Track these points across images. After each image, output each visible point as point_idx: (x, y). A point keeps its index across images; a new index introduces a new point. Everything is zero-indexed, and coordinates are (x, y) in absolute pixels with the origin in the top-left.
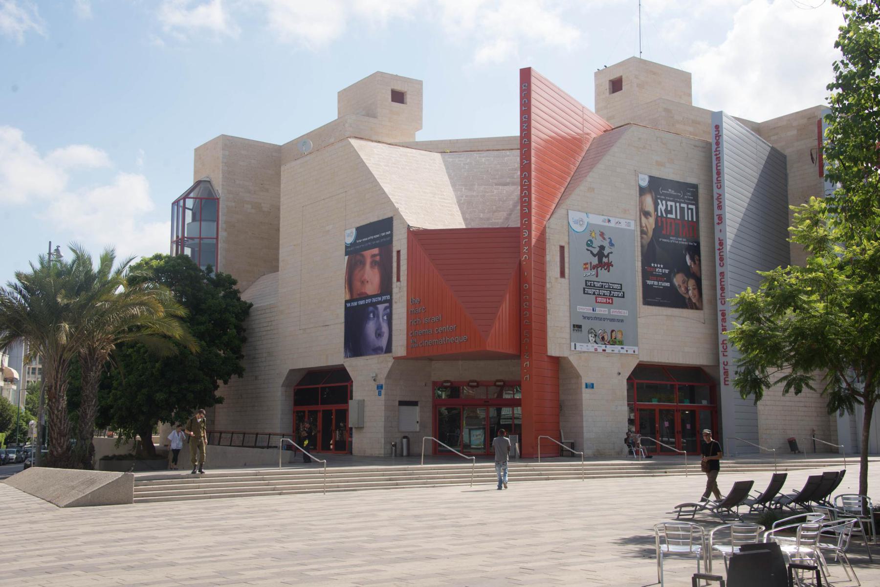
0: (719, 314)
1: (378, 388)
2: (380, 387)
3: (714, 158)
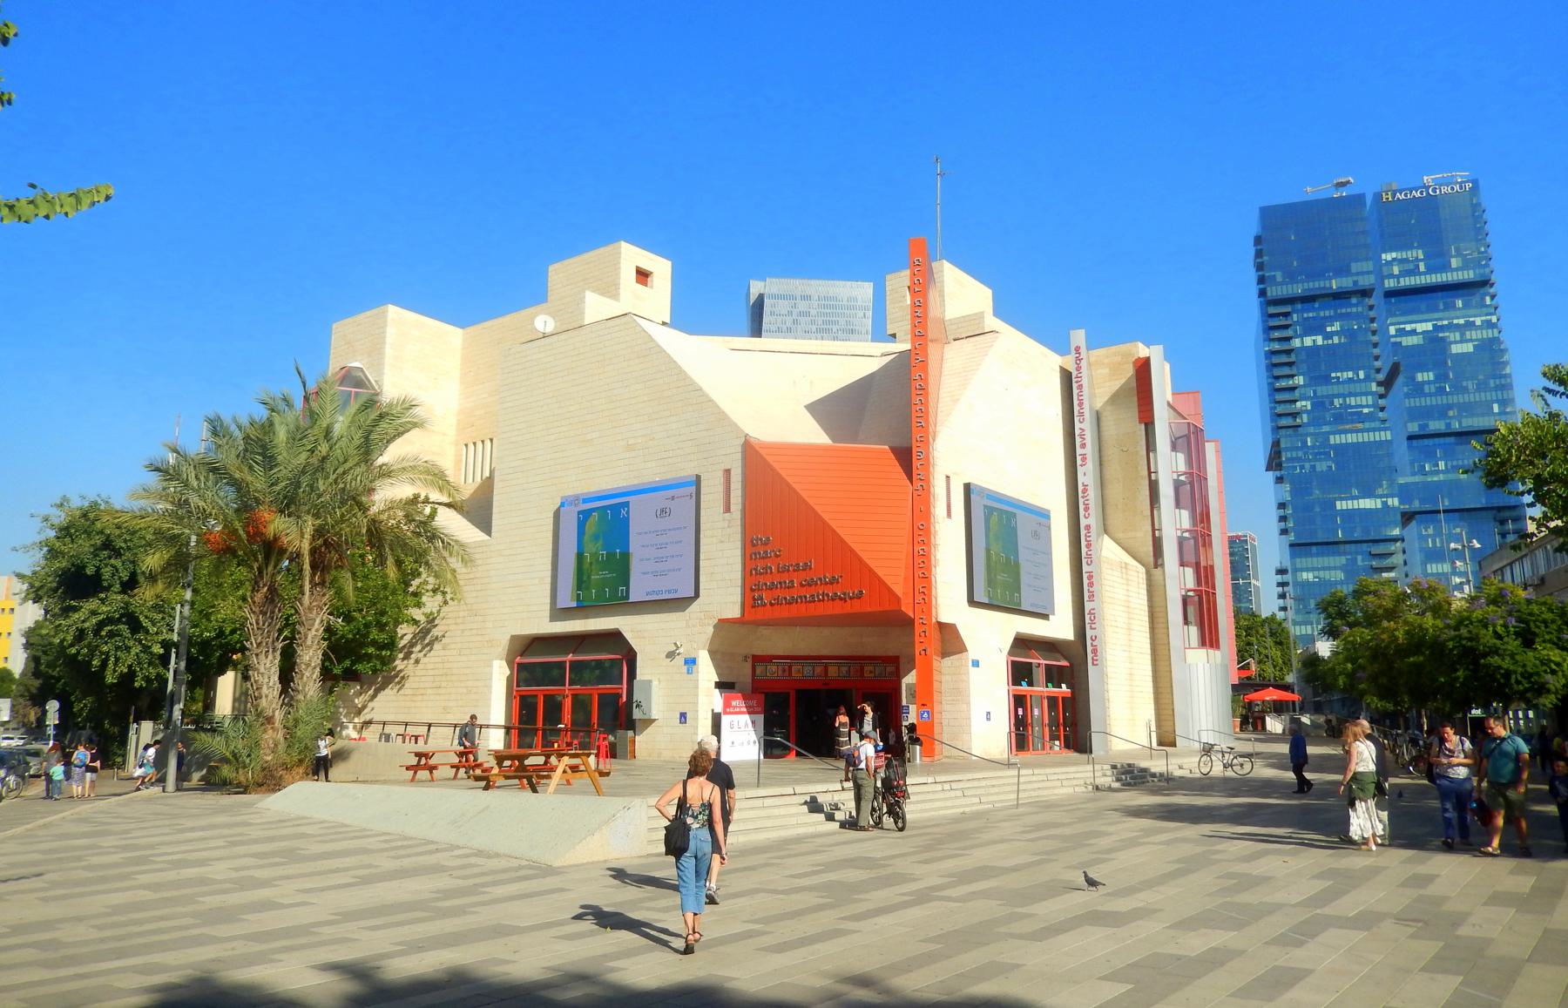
0: (1085, 576)
3: (1075, 386)
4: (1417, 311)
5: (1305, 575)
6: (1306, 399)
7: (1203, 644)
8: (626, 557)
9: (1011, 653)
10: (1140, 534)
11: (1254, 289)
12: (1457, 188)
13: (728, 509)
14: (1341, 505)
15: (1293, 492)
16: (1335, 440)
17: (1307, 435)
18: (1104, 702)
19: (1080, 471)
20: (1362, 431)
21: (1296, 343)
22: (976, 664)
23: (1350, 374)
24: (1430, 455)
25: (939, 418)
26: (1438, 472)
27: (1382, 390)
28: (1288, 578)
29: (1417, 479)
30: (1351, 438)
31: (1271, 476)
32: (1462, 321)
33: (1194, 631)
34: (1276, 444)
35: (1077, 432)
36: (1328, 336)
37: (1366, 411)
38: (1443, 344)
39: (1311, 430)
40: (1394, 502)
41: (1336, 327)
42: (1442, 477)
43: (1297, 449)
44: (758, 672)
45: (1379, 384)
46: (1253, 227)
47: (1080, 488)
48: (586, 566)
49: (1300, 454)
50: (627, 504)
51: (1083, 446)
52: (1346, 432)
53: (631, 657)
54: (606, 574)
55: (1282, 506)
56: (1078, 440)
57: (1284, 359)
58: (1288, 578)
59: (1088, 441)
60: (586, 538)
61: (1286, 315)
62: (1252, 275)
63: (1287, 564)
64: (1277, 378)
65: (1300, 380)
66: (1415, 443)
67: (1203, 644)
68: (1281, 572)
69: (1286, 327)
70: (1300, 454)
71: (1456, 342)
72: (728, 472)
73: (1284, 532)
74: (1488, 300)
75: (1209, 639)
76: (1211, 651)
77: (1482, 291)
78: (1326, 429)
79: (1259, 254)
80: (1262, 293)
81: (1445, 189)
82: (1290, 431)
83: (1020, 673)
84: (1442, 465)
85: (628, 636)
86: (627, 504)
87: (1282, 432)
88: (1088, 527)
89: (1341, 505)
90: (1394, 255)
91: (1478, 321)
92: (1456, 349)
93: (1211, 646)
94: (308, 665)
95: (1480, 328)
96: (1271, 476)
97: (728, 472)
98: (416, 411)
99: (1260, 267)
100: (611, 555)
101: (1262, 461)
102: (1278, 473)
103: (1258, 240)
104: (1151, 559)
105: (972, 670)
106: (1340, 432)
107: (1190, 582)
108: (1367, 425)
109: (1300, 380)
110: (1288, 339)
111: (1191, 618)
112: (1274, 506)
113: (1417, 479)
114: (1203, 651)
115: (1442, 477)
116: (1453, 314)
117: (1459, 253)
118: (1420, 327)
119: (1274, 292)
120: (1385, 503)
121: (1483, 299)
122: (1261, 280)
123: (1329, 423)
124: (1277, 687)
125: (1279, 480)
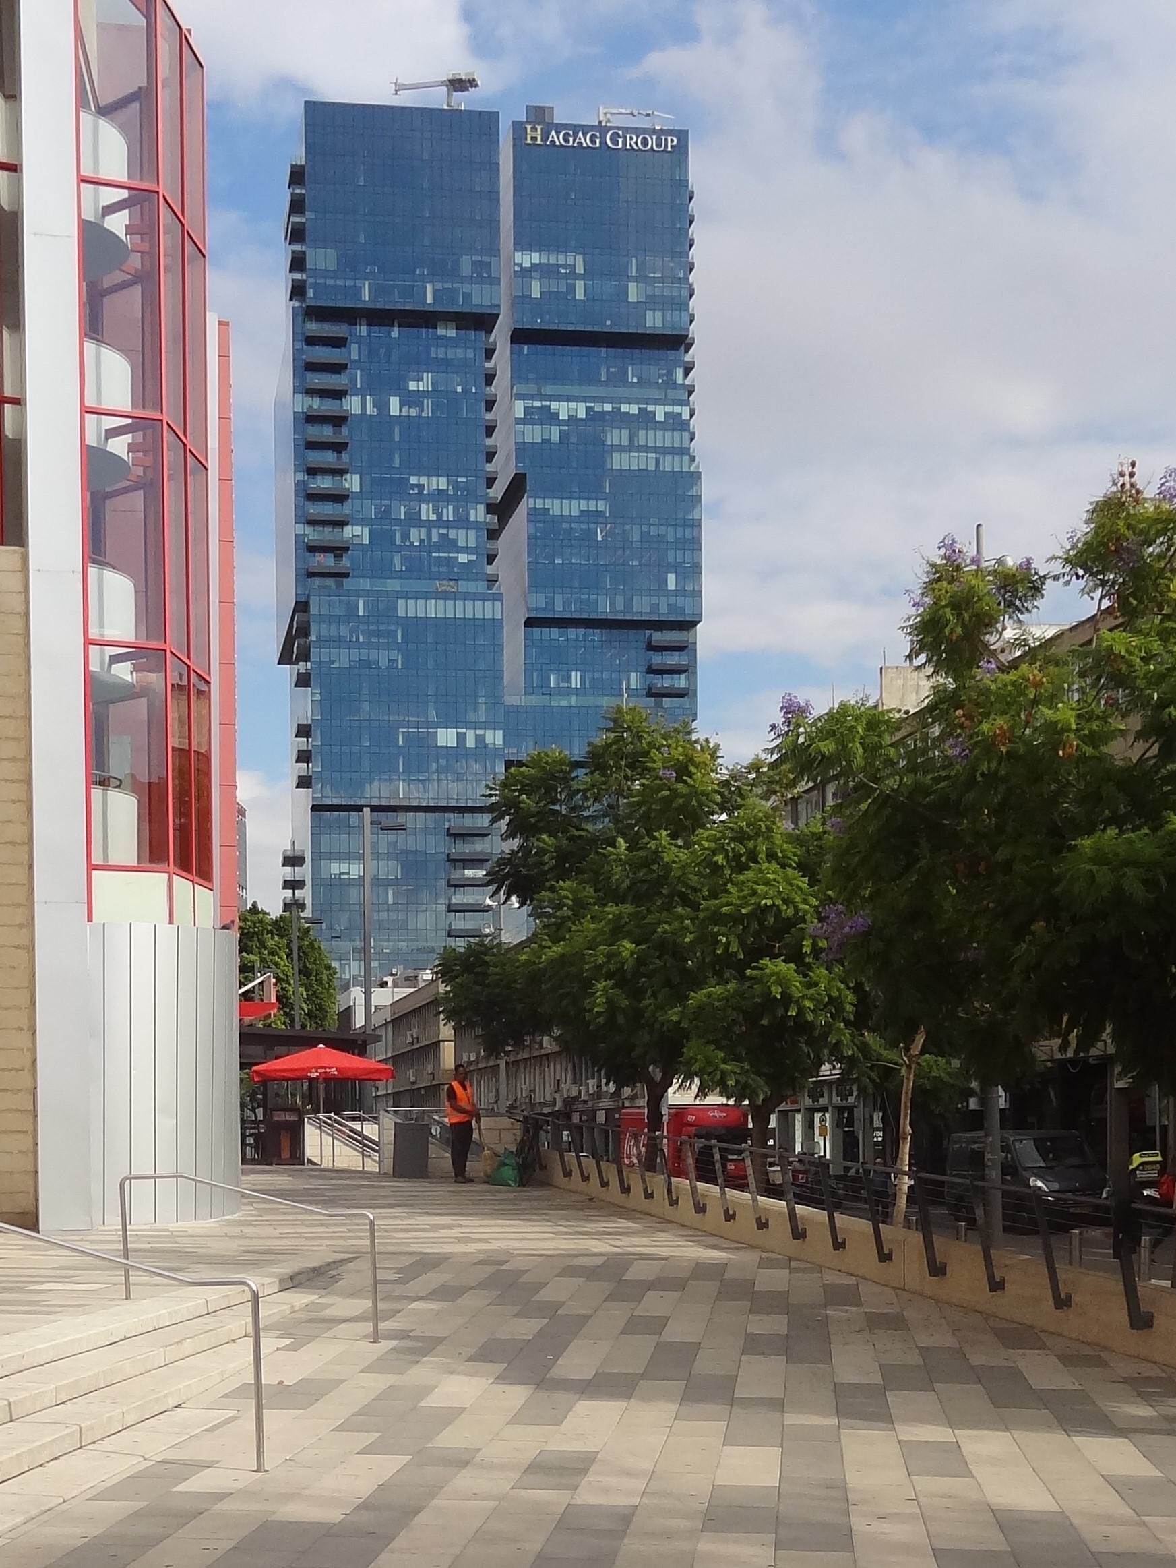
4: (558, 378)
5: (335, 868)
6: (362, 522)
7: (153, 852)
11: (282, 282)
12: (652, 142)
15: (327, 704)
16: (407, 609)
17: (358, 594)
20: (455, 596)
21: (353, 405)
24: (560, 661)
26: (569, 691)
27: (493, 520)
28: (304, 872)
29: (534, 700)
30: (434, 609)
31: (288, 672)
32: (634, 409)
33: (123, 810)
34: (301, 607)
36: (409, 399)
37: (463, 558)
38: (602, 450)
39: (365, 584)
40: (496, 738)
42: (574, 700)
43: (338, 620)
45: (490, 509)
49: (344, 630)
52: (426, 596)
55: (303, 731)
57: (326, 433)
58: (304, 872)
61: (339, 343)
64: (312, 472)
65: (353, 483)
66: (537, 632)
67: (153, 852)
68: (292, 860)
69: (339, 343)
70: (344, 630)
71: (620, 449)
74: (679, 372)
76: (182, 885)
77: (671, 354)
78: (393, 585)
79: (297, 206)
80: (297, 291)
81: (633, 141)
82: (330, 582)
84: (576, 679)
87: (317, 581)
90: (536, 258)
91: (660, 413)
92: (618, 461)
93: (184, 865)
95: (661, 426)
96: (288, 672)
99: (296, 234)
102: (302, 667)
103: (297, 176)
106: (417, 596)
107: (120, 616)
108: (463, 586)
109: (353, 483)
110: (338, 394)
111: (120, 760)
113: (534, 700)
114: (155, 882)
115: (574, 700)
116: (622, 392)
117: (641, 278)
118: (563, 410)
120: (480, 739)
121: (670, 373)
123: (400, 576)
124: (333, 1043)
125: (303, 681)
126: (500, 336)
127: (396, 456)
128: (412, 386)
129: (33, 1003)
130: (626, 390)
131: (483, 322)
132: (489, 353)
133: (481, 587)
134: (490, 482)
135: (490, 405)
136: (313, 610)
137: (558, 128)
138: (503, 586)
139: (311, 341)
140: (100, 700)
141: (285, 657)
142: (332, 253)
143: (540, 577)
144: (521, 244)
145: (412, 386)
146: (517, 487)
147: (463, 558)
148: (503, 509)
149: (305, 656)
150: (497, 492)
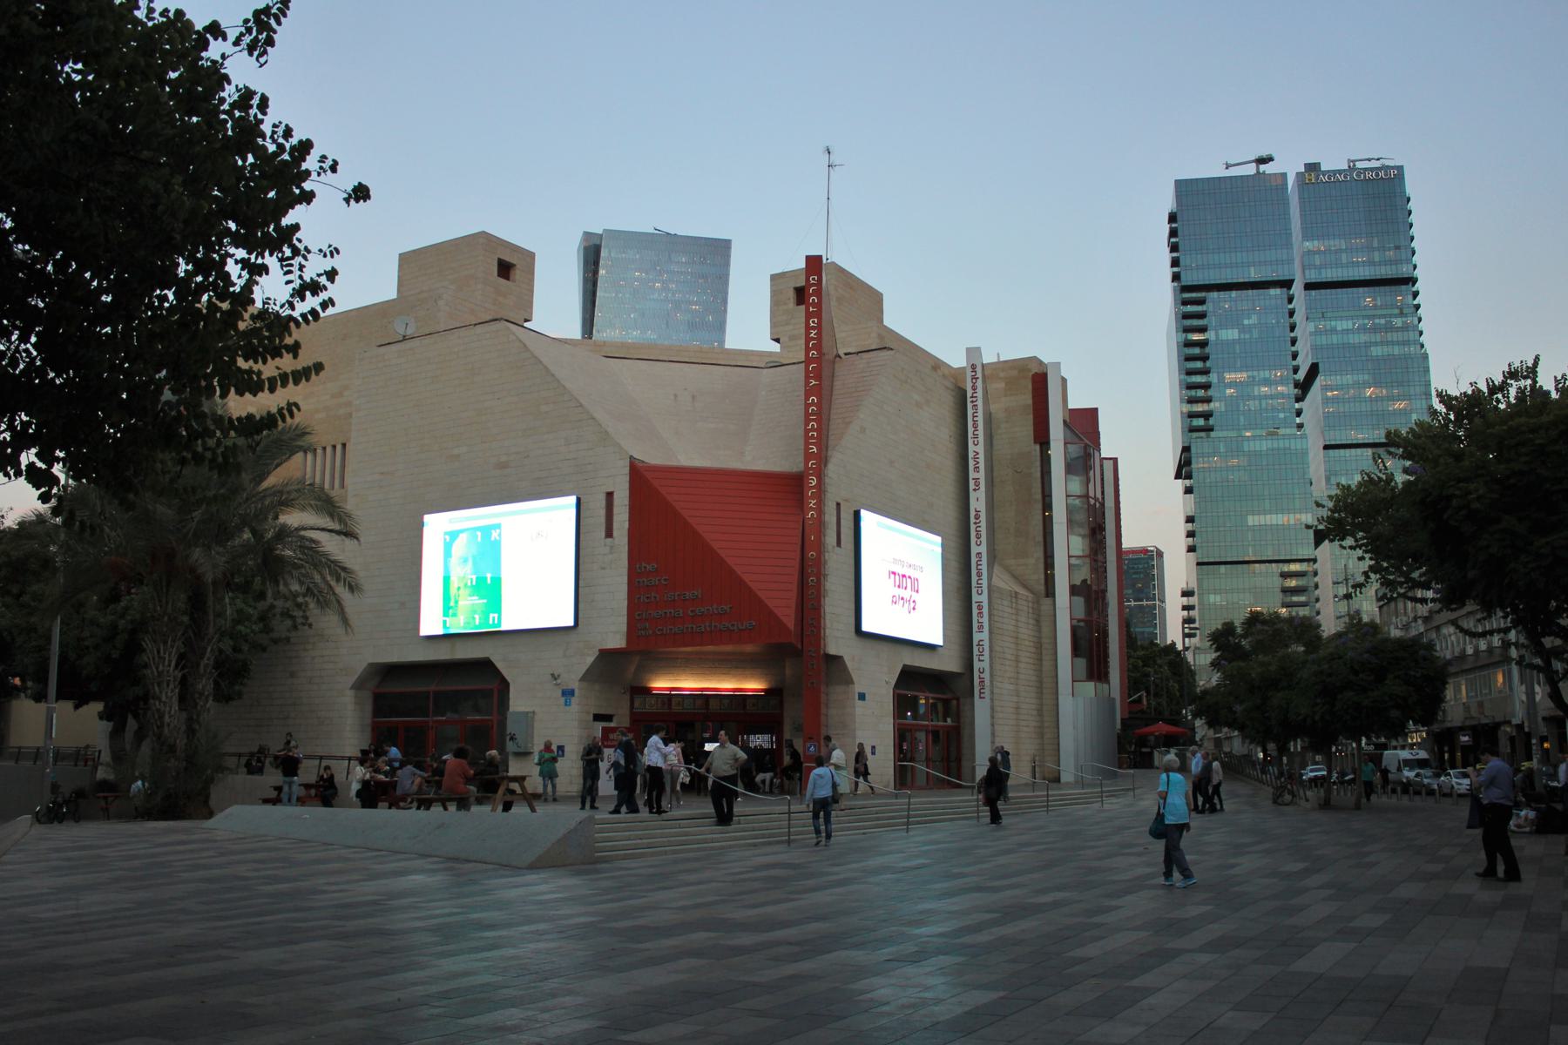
0: (975, 606)
1: (564, 693)
2: (568, 693)
3: (969, 406)
5: (1212, 598)
8: (497, 581)
9: (897, 685)
10: (1032, 561)
11: (1168, 272)
13: (609, 533)
14: (1252, 520)
18: (972, 736)
19: (973, 495)
22: (862, 697)
23: (1267, 374)
25: (831, 443)
28: (1193, 600)
35: (971, 455)
36: (1243, 329)
41: (1254, 320)
44: (637, 704)
45: (1297, 385)
46: (1168, 203)
47: (972, 514)
48: (453, 591)
50: (498, 526)
51: (976, 469)
53: (504, 685)
54: (476, 600)
55: (1190, 520)
56: (971, 463)
58: (1193, 600)
59: (982, 465)
60: (454, 561)
62: (1166, 256)
63: (1193, 585)
68: (1186, 594)
69: (1202, 302)
72: (610, 495)
73: (1191, 549)
75: (1097, 672)
79: (1173, 233)
82: (1203, 434)
83: (903, 704)
85: (499, 665)
86: (498, 526)
87: (1195, 435)
88: (976, 479)
89: (1252, 520)
94: (201, 694)
95: (1398, 329)
97: (610, 495)
98: (307, 438)
99: (1174, 248)
100: (481, 580)
101: (1172, 469)
102: (1188, 483)
103: (1172, 218)
104: (1042, 588)
105: (859, 703)
112: (1183, 520)
114: (1091, 684)
119: (1188, 279)
122: (1175, 263)
125: (1188, 491)
126: (1297, 289)
127: (1071, 954)
128: (1246, 322)
129: (1056, 653)
130: (1401, 296)
131: (1287, 284)
132: (1290, 300)
133: (1294, 431)
134: (1296, 370)
135: (1293, 328)
136: (1193, 450)
137: (1324, 173)
138: (1307, 429)
139: (1185, 303)
140: (1070, 511)
141: (1178, 476)
142: (1250, 523)
143: (1330, 421)
144: (1306, 237)
145: (1246, 322)
146: (1314, 371)
147: (1281, 415)
148: (1304, 387)
149: (1189, 477)
150: (1301, 376)
